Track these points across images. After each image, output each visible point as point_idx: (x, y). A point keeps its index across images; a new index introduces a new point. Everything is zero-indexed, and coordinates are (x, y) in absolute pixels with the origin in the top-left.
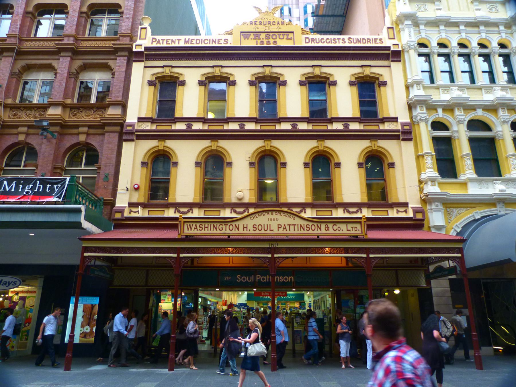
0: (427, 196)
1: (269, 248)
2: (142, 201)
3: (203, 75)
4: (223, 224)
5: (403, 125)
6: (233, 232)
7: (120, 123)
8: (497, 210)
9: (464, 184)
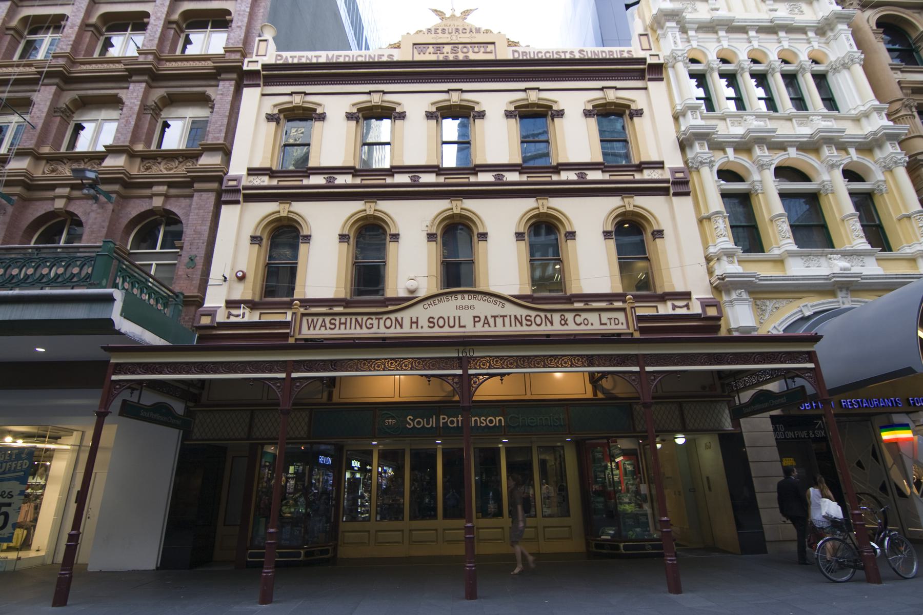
0: (723, 279)
1: (459, 358)
2: (249, 297)
3: (354, 105)
4: (374, 317)
5: (674, 171)
6: (392, 330)
7: (217, 177)
8: (838, 302)
9: (779, 262)
